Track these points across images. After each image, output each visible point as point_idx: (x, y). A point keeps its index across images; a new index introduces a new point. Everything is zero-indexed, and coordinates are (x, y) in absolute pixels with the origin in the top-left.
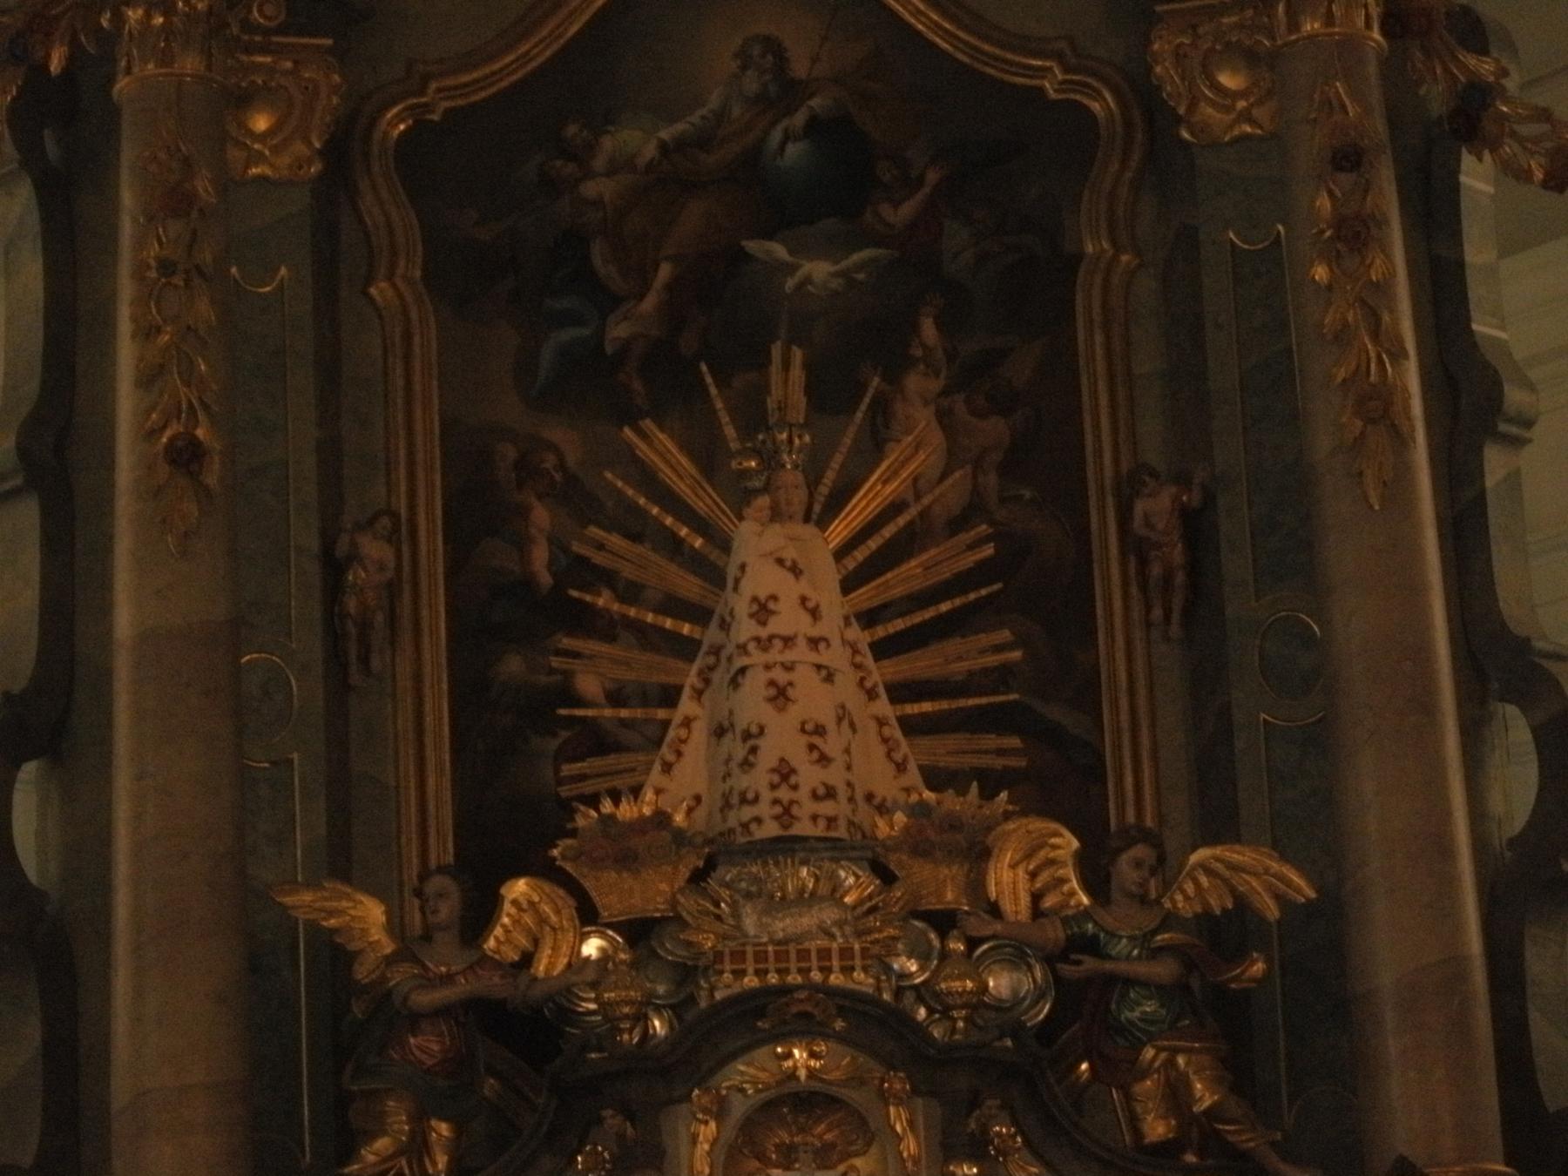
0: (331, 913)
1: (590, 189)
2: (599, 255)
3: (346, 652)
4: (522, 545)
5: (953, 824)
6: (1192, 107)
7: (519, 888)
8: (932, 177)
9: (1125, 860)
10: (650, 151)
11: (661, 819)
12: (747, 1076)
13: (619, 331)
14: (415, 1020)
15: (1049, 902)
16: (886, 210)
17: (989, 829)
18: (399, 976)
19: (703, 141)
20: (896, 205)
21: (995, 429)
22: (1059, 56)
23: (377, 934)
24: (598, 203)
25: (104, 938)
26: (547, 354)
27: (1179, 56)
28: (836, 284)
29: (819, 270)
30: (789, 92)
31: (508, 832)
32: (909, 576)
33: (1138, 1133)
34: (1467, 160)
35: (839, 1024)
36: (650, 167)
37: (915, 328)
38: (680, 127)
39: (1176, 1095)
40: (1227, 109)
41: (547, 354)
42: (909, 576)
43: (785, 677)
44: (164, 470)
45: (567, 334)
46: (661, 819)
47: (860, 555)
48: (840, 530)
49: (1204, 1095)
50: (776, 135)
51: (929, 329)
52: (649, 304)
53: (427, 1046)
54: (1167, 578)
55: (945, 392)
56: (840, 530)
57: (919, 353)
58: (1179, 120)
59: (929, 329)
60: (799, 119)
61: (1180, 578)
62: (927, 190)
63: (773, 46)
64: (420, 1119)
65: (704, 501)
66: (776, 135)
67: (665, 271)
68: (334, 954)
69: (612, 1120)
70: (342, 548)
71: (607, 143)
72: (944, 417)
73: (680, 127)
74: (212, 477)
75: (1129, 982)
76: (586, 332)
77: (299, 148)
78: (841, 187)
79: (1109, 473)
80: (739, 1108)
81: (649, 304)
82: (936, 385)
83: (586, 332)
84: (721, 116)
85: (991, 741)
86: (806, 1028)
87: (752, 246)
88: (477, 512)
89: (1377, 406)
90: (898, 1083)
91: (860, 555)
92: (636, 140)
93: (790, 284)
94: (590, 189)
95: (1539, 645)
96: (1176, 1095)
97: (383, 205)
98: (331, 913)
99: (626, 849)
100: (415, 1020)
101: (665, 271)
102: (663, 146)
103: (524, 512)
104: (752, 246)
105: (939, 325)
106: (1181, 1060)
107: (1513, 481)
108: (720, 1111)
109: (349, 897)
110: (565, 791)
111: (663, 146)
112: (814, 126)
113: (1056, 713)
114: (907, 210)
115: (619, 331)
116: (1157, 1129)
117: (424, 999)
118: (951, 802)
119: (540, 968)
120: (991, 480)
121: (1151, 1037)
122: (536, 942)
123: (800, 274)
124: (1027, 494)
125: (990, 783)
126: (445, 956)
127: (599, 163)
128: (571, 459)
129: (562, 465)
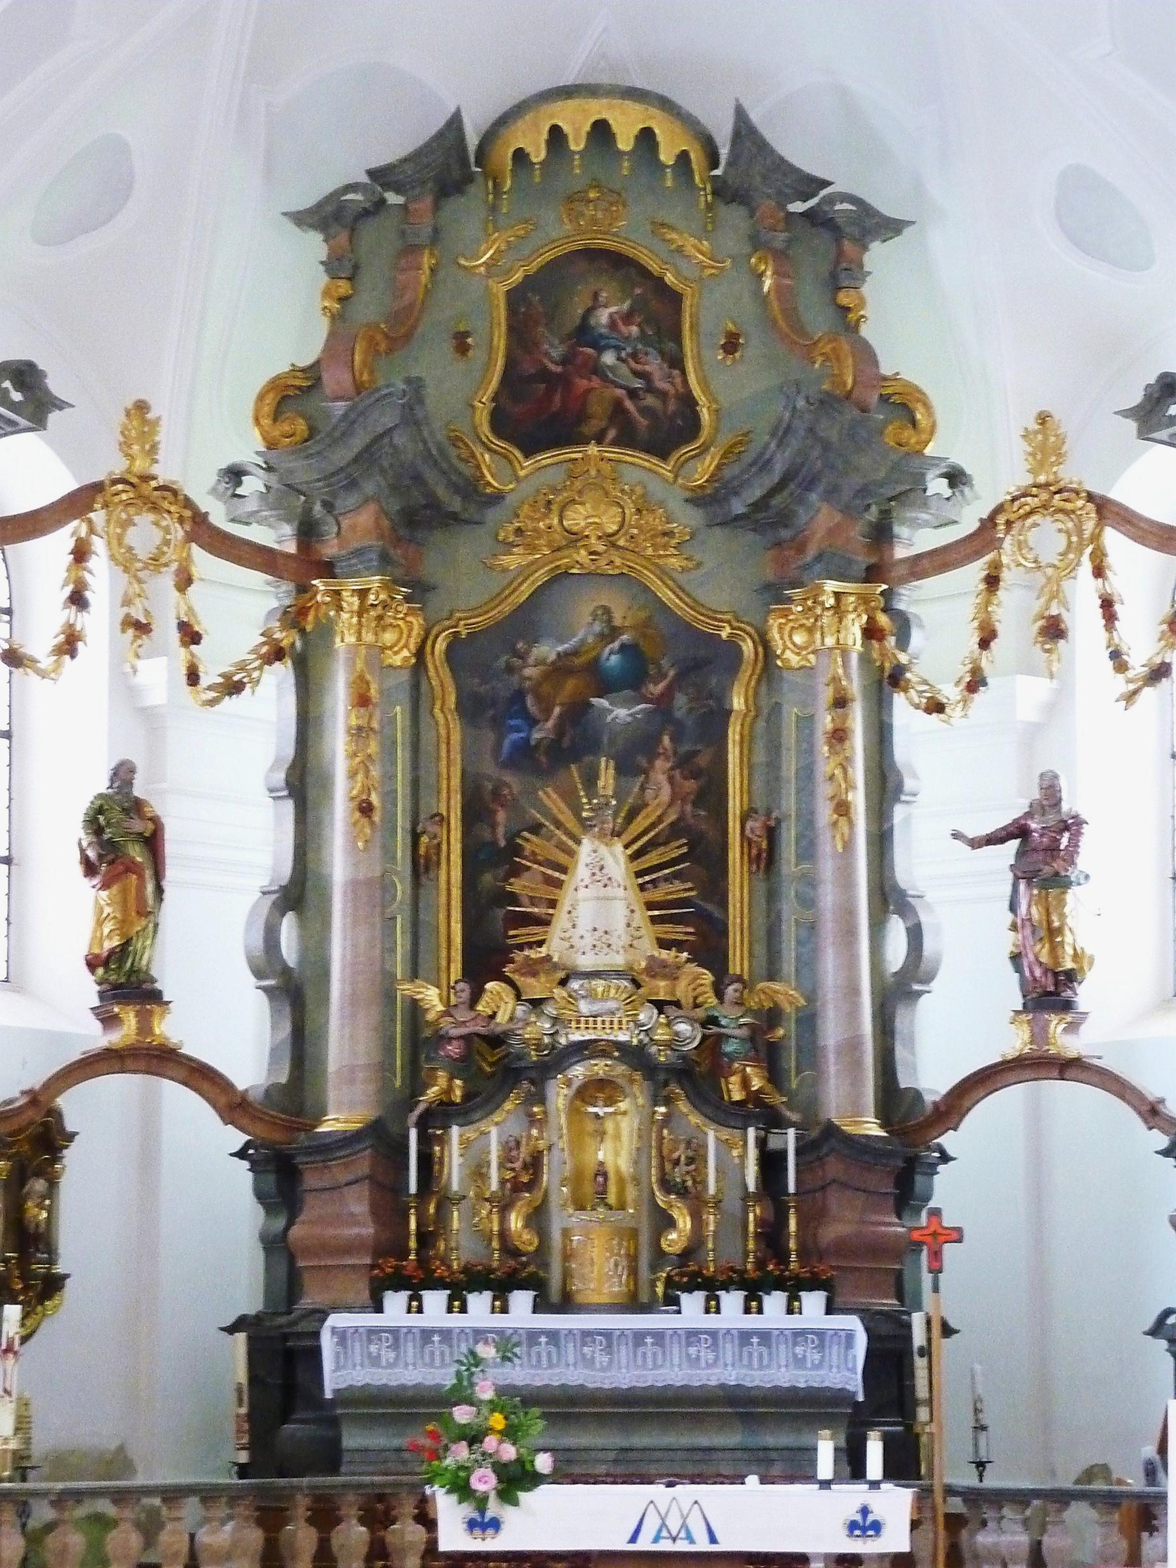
0: (419, 993)
1: (528, 672)
2: (530, 701)
3: (422, 867)
4: (493, 826)
5: (664, 964)
6: (783, 652)
7: (489, 986)
8: (672, 673)
9: (731, 988)
10: (552, 657)
11: (548, 958)
12: (579, 1072)
13: (537, 735)
14: (450, 1039)
15: (700, 1000)
16: (651, 687)
17: (678, 968)
18: (445, 1023)
19: (575, 653)
20: (656, 684)
21: (691, 785)
22: (729, 622)
23: (436, 1001)
24: (529, 679)
25: (325, 999)
26: (507, 744)
27: (781, 628)
28: (629, 719)
29: (622, 713)
30: (612, 632)
31: (485, 961)
32: (652, 859)
33: (730, 1097)
34: (895, 695)
35: (616, 1054)
36: (553, 663)
37: (660, 741)
38: (566, 646)
39: (745, 1083)
40: (798, 654)
41: (507, 744)
42: (652, 859)
43: (598, 907)
44: (358, 814)
45: (515, 736)
46: (548, 958)
47: (635, 847)
48: (627, 837)
49: (756, 1084)
50: (607, 650)
51: (666, 740)
52: (550, 724)
53: (453, 1049)
54: (759, 855)
55: (672, 769)
56: (627, 837)
57: (661, 751)
58: (778, 657)
59: (666, 740)
60: (616, 645)
61: (764, 855)
62: (669, 679)
63: (607, 611)
64: (451, 1079)
65: (571, 824)
66: (607, 650)
67: (557, 710)
68: (415, 1008)
69: (525, 1085)
70: (419, 829)
71: (535, 651)
72: (671, 780)
73: (566, 646)
74: (377, 818)
75: (729, 1037)
76: (522, 735)
77: (405, 653)
78: (635, 675)
79: (738, 812)
80: (576, 1084)
81: (550, 724)
82: (669, 765)
83: (522, 735)
84: (583, 642)
85: (681, 928)
86: (604, 1054)
87: (594, 700)
88: (476, 810)
89: (843, 809)
90: (638, 1076)
91: (635, 847)
92: (547, 650)
93: (609, 718)
94: (528, 672)
95: (910, 892)
96: (745, 1083)
97: (439, 673)
98: (419, 993)
99: (532, 969)
100: (450, 1039)
101: (557, 710)
102: (559, 654)
103: (495, 812)
104: (594, 700)
105: (671, 739)
106: (748, 1069)
107: (907, 820)
108: (568, 1083)
109: (424, 987)
110: (510, 942)
111: (559, 654)
112: (623, 647)
113: (710, 907)
114: (661, 686)
115: (537, 735)
116: (737, 1096)
117: (454, 1032)
118: (664, 954)
119: (498, 1019)
120: (689, 808)
121: (737, 1059)
122: (498, 1007)
123: (612, 716)
124: (768, 283)
125: (679, 945)
126: (463, 1015)
127: (531, 660)
128: (515, 791)
129: (511, 794)
